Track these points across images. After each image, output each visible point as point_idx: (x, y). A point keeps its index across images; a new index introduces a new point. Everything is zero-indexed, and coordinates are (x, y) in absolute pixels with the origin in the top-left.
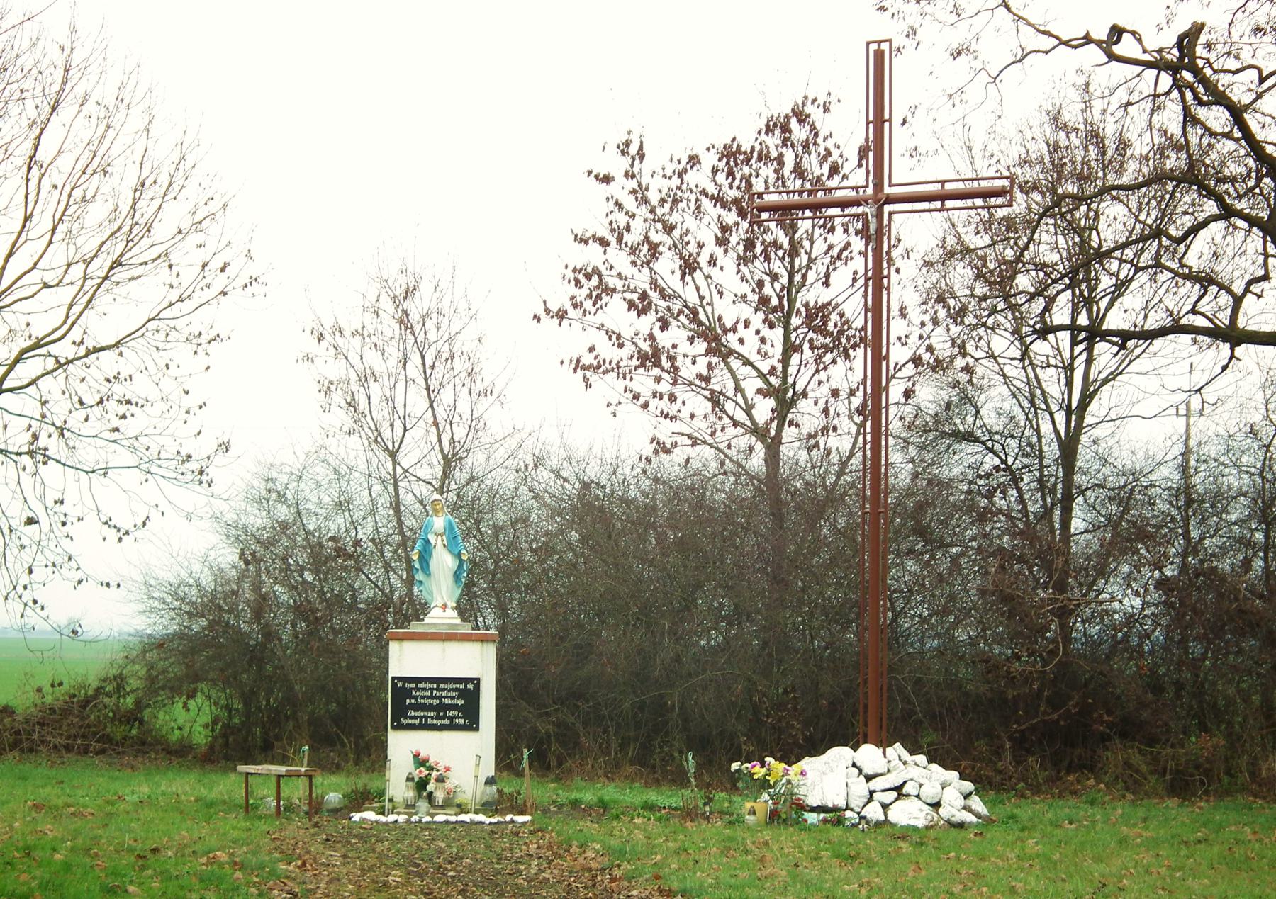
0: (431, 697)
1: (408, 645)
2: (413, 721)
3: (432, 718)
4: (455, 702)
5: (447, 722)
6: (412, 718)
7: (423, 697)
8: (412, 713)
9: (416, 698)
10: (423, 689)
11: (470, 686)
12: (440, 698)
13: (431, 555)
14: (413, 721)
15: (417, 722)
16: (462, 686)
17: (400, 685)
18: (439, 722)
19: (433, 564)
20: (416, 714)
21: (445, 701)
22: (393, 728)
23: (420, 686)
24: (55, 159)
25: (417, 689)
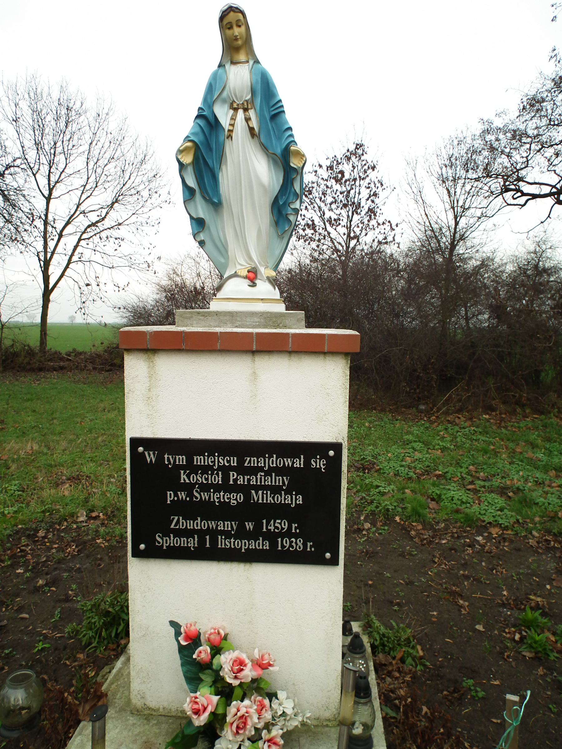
0: (226, 487)
1: (169, 366)
2: (183, 542)
3: (227, 535)
4: (283, 499)
5: (263, 545)
6: (179, 533)
7: (205, 488)
8: (178, 522)
9: (189, 488)
10: (205, 469)
11: (319, 464)
12: (246, 489)
13: (221, 157)
14: (183, 542)
15: (192, 543)
16: (299, 463)
17: (151, 457)
18: (244, 545)
19: (227, 178)
20: (190, 525)
21: (258, 497)
22: (137, 554)
23: (198, 460)
24: (47, 209)
25: (192, 468)
